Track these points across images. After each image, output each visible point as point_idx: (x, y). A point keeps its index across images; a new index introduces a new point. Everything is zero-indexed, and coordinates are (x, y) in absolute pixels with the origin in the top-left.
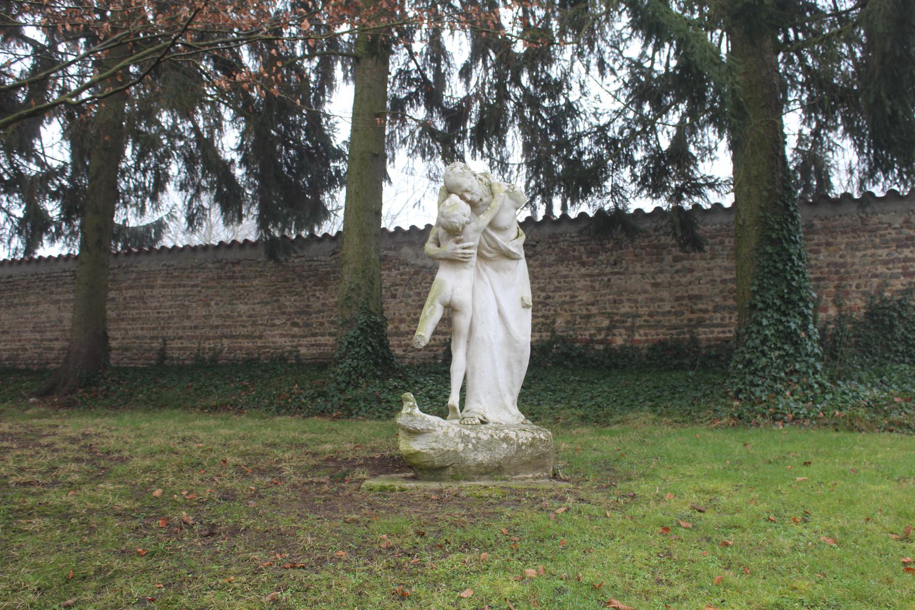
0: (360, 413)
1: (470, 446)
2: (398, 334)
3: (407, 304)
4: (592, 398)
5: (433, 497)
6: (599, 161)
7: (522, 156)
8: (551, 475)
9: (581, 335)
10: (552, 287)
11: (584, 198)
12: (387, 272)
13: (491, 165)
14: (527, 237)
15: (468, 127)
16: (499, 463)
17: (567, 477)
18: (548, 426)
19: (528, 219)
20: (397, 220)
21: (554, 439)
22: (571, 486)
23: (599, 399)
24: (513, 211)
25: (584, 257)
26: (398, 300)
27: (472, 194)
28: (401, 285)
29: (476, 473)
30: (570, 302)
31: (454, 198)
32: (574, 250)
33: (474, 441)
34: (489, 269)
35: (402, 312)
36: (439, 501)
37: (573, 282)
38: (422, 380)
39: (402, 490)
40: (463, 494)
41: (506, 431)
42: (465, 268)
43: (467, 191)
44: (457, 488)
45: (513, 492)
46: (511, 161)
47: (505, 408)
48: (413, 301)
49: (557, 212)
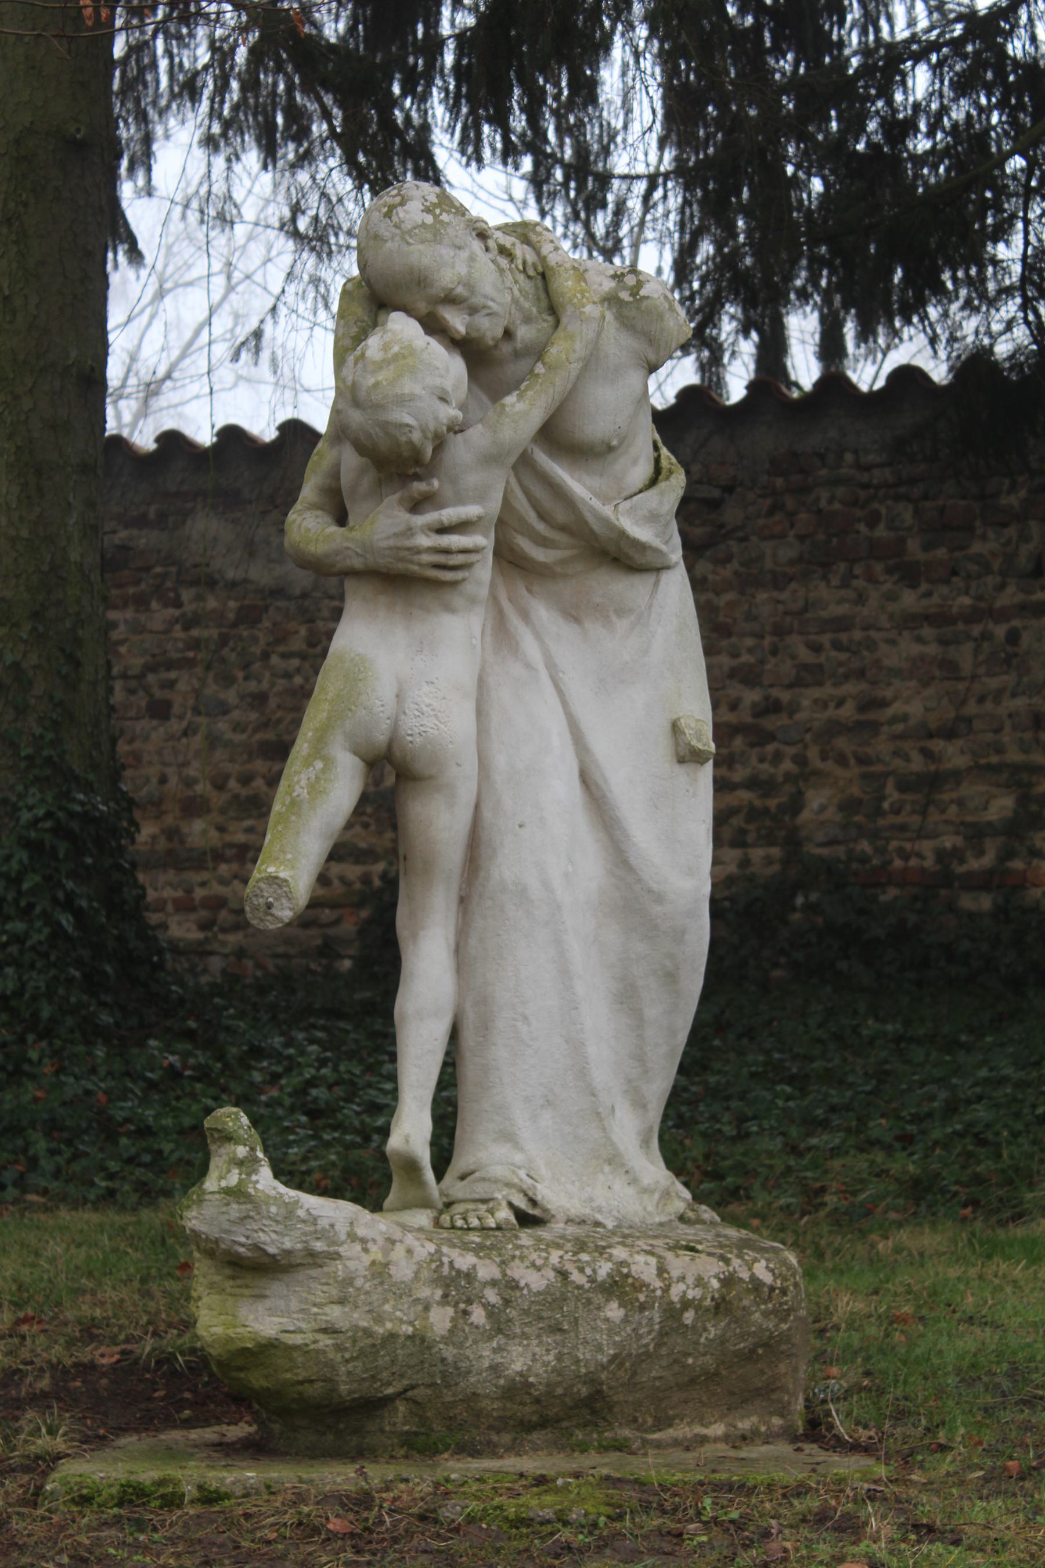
0: (33, 1179)
1: (478, 1315)
2: (179, 858)
3: (213, 741)
4: (951, 1109)
5: (335, 1525)
6: (971, 149)
7: (662, 144)
8: (800, 1426)
9: (905, 856)
10: (787, 668)
11: (912, 308)
12: (129, 614)
13: (538, 181)
14: (688, 473)
15: (446, 29)
16: (591, 1380)
17: (863, 1434)
18: (781, 1226)
19: (687, 395)
20: (169, 396)
21: (809, 1275)
22: (882, 1471)
23: (981, 1113)
24: (634, 377)
25: (913, 545)
26: (175, 726)
27: (473, 310)
28: (190, 663)
29: (502, 1424)
30: (860, 725)
31: (402, 327)
32: (873, 521)
33: (492, 1296)
34: (542, 612)
35: (192, 772)
36: (359, 1539)
37: (871, 645)
38: (277, 1041)
39: (209, 1497)
40: (452, 1511)
41: (620, 1253)
42: (449, 609)
43: (451, 300)
44: (426, 1488)
45: (652, 1497)
46: (620, 163)
47: (615, 1160)
48: (238, 727)
49: (804, 368)
